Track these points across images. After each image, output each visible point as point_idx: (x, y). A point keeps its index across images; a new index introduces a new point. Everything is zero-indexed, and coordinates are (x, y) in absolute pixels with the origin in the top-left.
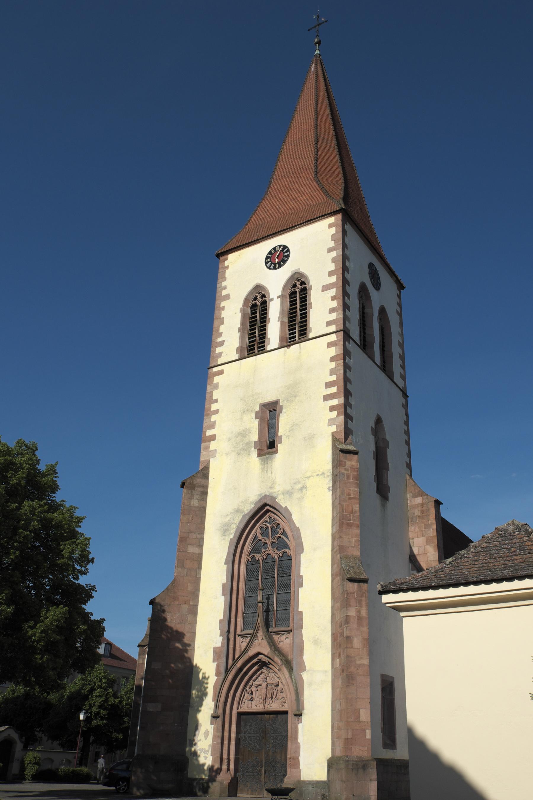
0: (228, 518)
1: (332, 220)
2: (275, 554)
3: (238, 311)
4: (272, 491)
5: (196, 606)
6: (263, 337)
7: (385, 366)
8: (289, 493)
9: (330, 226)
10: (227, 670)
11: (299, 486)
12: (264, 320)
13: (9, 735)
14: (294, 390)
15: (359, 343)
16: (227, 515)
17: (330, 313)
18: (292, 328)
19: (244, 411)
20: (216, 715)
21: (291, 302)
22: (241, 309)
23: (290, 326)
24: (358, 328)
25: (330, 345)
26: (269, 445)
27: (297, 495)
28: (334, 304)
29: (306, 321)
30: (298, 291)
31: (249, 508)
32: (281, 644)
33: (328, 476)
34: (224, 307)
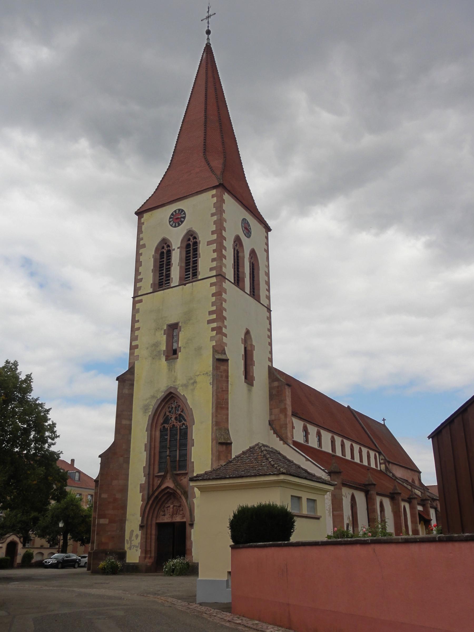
0: (148, 401)
1: (214, 192)
2: (178, 424)
3: (152, 257)
4: (175, 384)
5: (129, 458)
6: (168, 276)
7: (254, 293)
8: (185, 386)
9: (213, 196)
10: (149, 498)
11: (192, 381)
12: (169, 264)
13: (13, 539)
14: (189, 316)
15: (233, 281)
16: (147, 399)
17: (212, 262)
18: (187, 270)
19: (157, 329)
20: (143, 524)
21: (186, 251)
22: (153, 255)
23: (186, 269)
24: (232, 270)
25: (212, 285)
26: (172, 354)
27: (191, 387)
28: (215, 255)
29: (196, 266)
30: (191, 243)
31: (160, 395)
32: (182, 481)
33: (210, 375)
34: (142, 253)
